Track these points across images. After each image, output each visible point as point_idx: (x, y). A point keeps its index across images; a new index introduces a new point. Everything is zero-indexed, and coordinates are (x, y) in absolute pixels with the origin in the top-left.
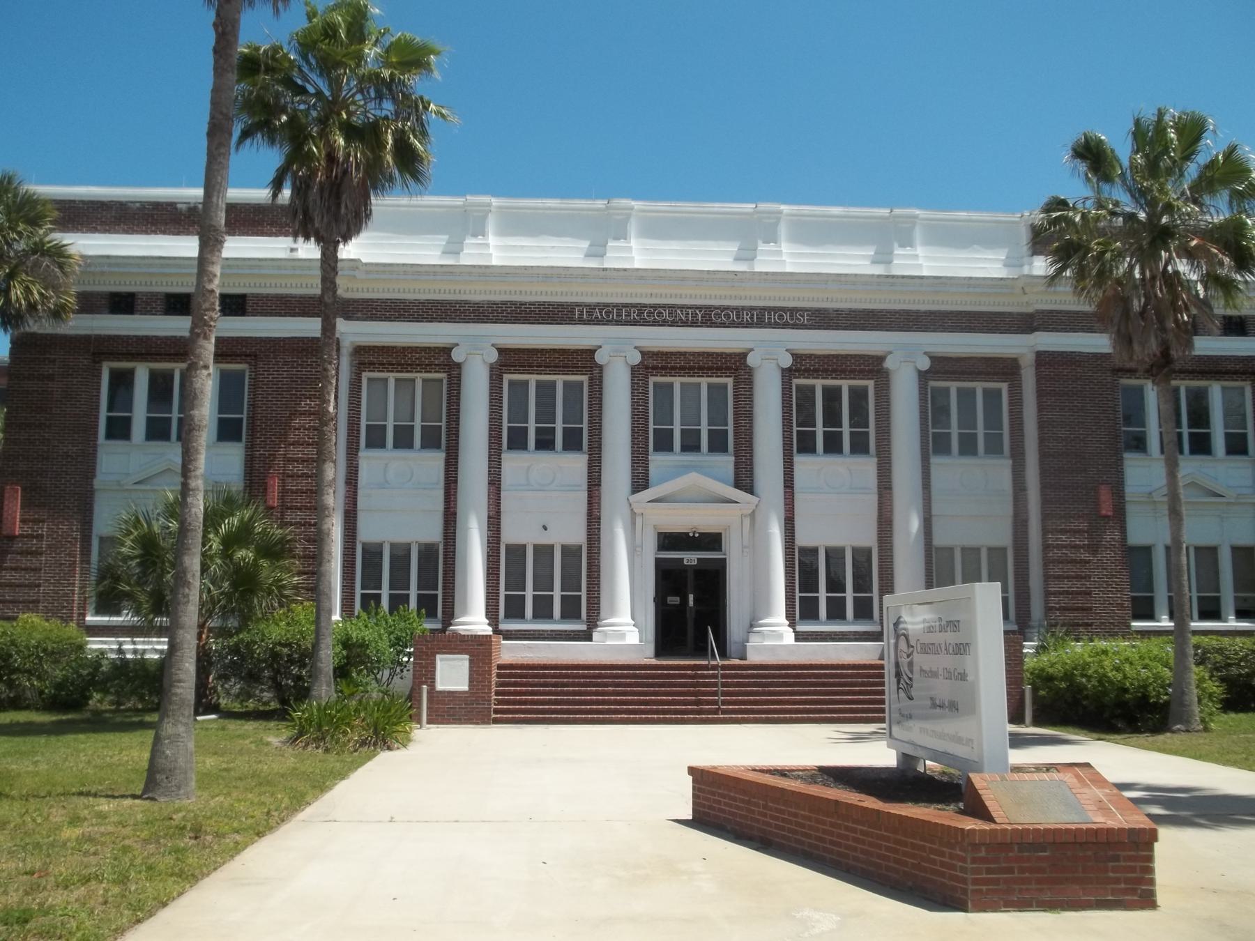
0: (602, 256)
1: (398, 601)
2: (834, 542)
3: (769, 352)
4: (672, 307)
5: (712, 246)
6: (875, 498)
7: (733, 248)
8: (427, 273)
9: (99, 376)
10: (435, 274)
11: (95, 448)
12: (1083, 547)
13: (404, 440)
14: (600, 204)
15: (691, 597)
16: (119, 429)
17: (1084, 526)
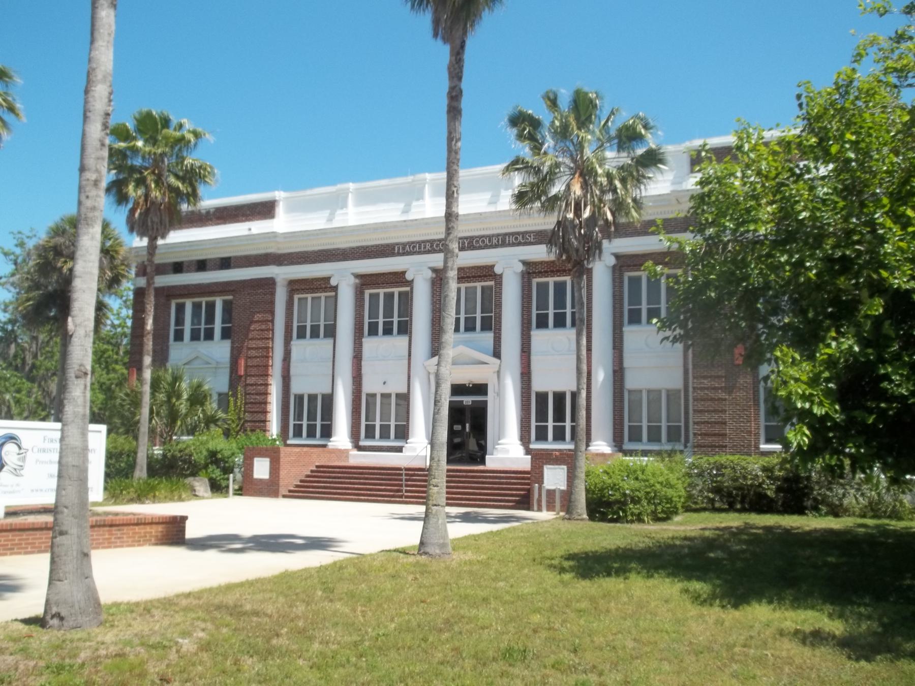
2: (559, 388)
9: (169, 308)
10: (335, 232)
11: (168, 347)
12: (721, 388)
14: (410, 178)
15: (467, 425)
16: (179, 336)
17: (722, 373)
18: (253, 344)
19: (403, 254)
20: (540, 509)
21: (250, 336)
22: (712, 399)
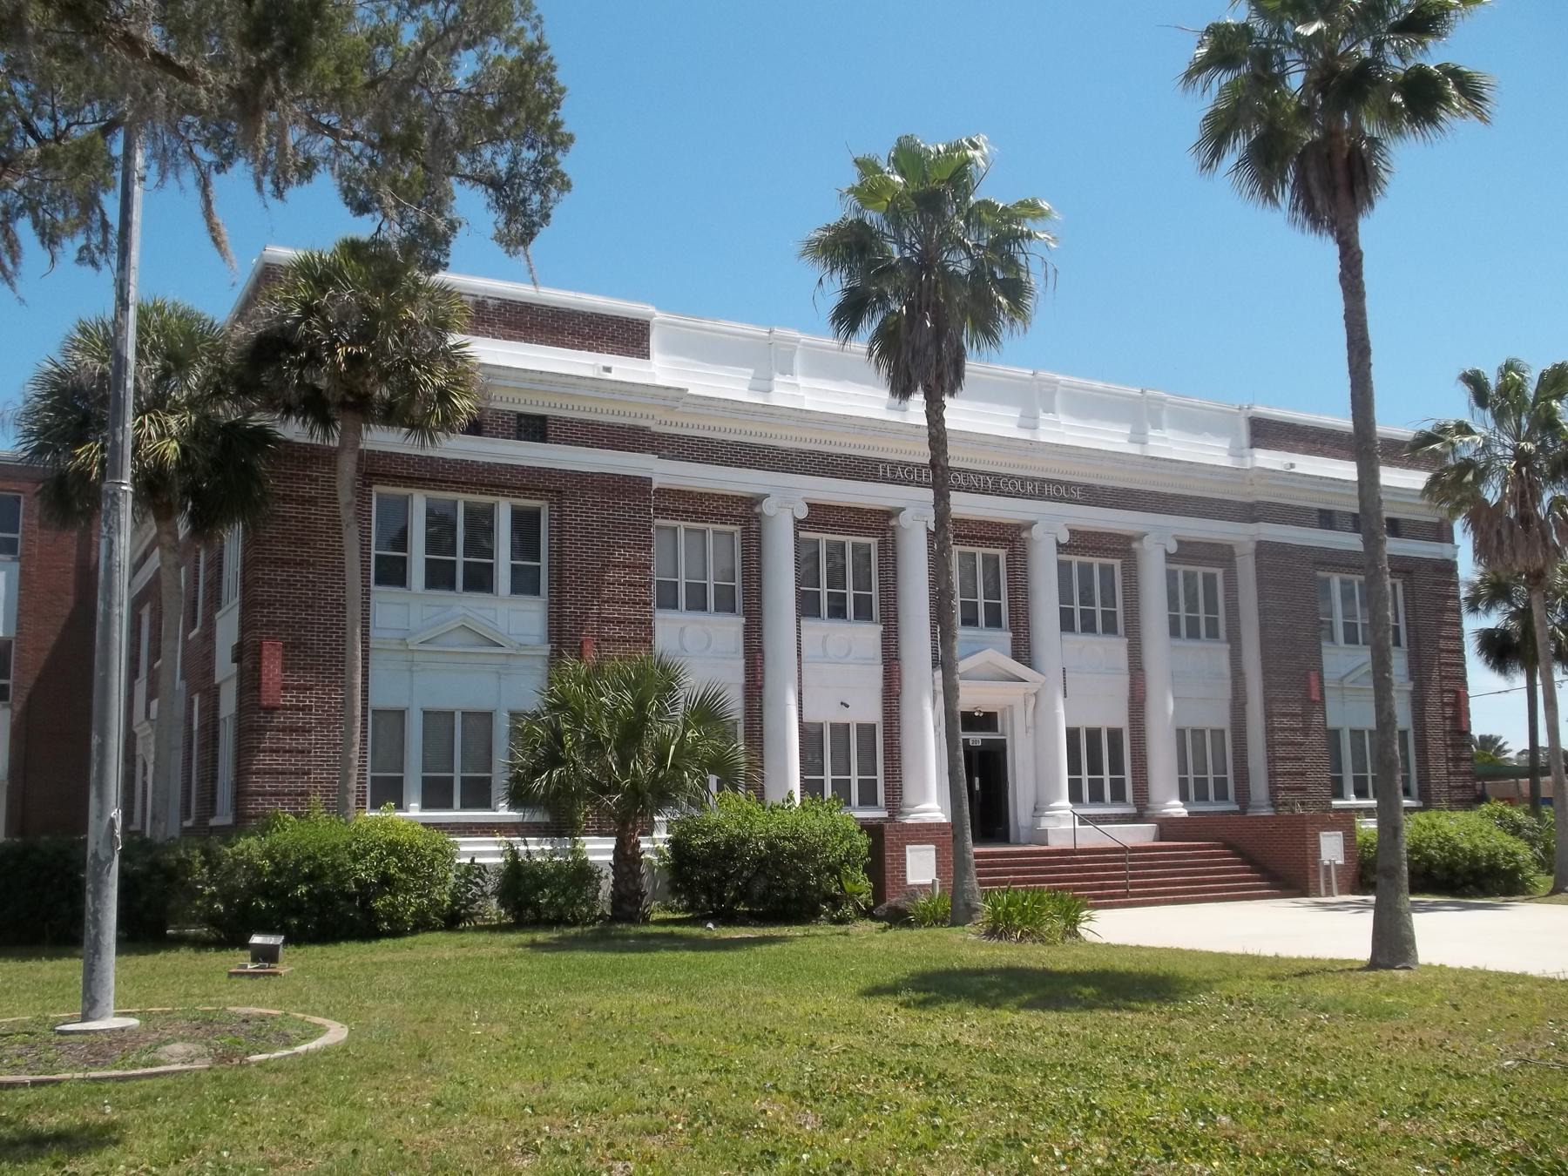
0: (769, 391)
1: (842, 788)
3: (786, 498)
4: (966, 471)
5: (997, 409)
6: (1126, 678)
7: (748, 373)
8: (746, 412)
13: (697, 602)
16: (393, 573)
17: (1298, 710)
18: (609, 611)
19: (893, 481)
20: (1329, 893)
21: (606, 594)
22: (1292, 744)
